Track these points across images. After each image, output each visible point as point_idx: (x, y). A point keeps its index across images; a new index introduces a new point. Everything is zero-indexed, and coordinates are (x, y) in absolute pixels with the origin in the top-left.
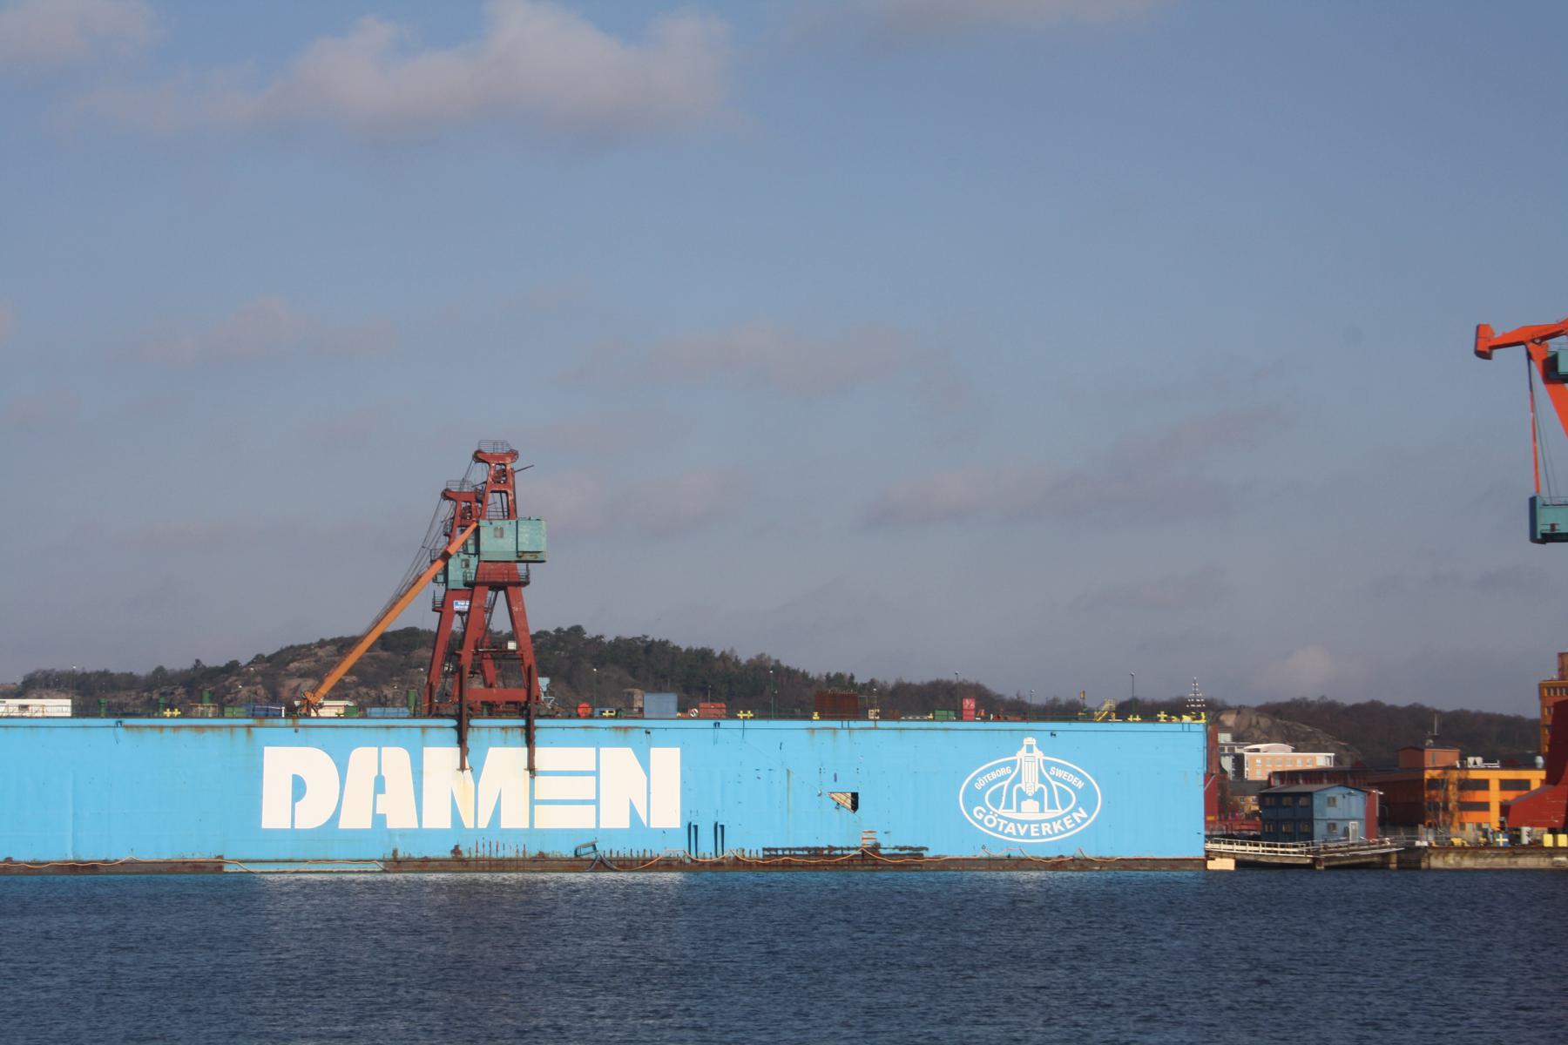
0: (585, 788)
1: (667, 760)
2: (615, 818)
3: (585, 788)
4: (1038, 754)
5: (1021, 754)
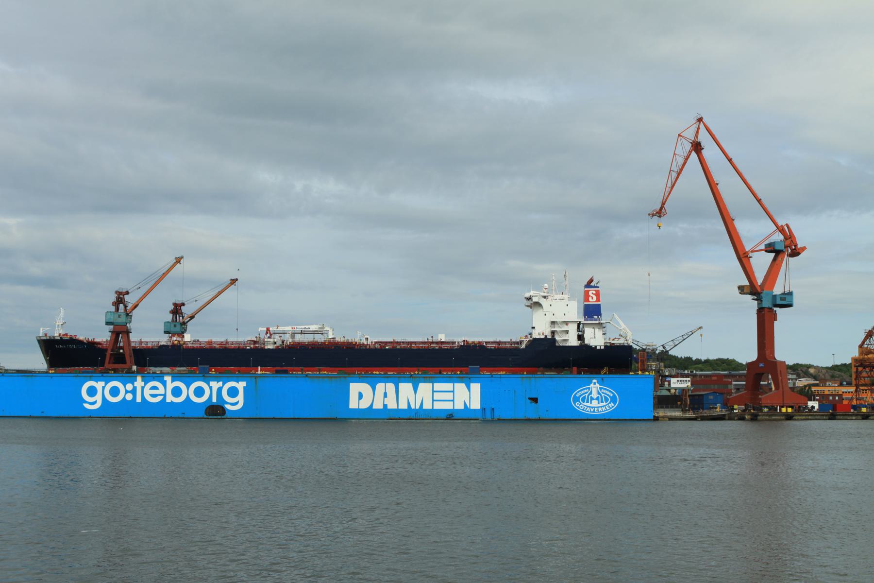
0: (449, 396)
1: (476, 387)
2: (459, 406)
3: (449, 396)
4: (597, 385)
5: (592, 385)
